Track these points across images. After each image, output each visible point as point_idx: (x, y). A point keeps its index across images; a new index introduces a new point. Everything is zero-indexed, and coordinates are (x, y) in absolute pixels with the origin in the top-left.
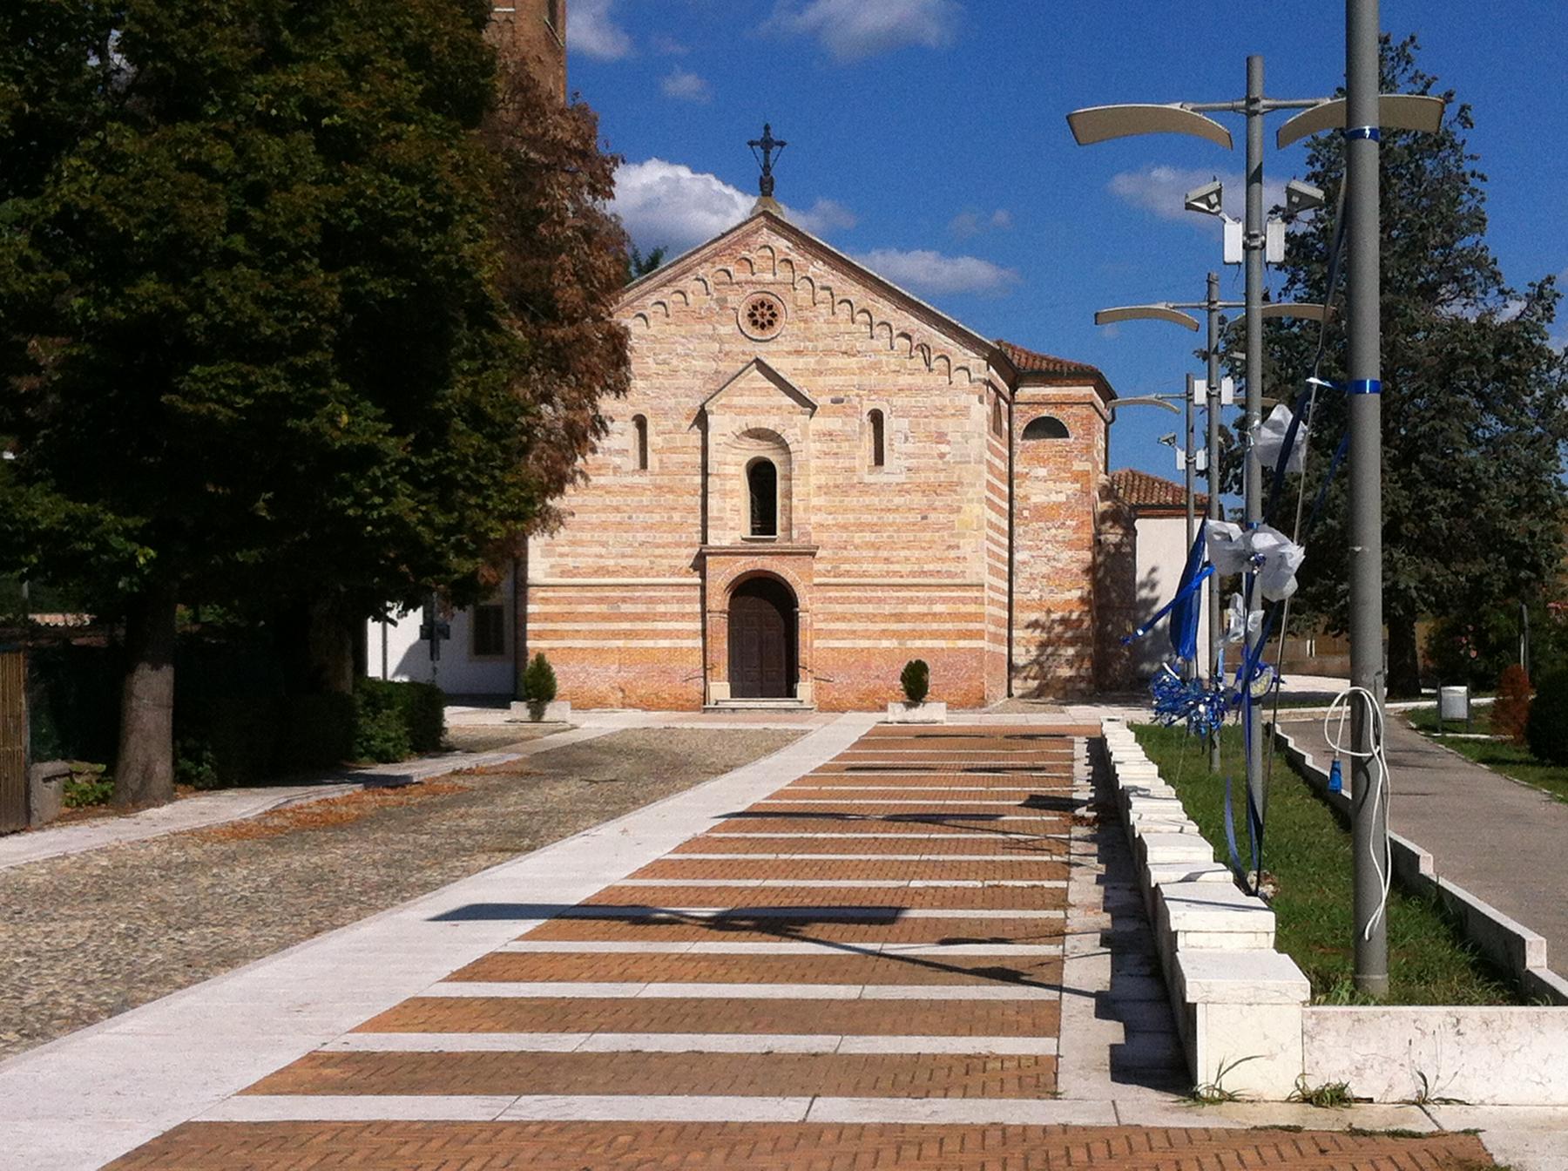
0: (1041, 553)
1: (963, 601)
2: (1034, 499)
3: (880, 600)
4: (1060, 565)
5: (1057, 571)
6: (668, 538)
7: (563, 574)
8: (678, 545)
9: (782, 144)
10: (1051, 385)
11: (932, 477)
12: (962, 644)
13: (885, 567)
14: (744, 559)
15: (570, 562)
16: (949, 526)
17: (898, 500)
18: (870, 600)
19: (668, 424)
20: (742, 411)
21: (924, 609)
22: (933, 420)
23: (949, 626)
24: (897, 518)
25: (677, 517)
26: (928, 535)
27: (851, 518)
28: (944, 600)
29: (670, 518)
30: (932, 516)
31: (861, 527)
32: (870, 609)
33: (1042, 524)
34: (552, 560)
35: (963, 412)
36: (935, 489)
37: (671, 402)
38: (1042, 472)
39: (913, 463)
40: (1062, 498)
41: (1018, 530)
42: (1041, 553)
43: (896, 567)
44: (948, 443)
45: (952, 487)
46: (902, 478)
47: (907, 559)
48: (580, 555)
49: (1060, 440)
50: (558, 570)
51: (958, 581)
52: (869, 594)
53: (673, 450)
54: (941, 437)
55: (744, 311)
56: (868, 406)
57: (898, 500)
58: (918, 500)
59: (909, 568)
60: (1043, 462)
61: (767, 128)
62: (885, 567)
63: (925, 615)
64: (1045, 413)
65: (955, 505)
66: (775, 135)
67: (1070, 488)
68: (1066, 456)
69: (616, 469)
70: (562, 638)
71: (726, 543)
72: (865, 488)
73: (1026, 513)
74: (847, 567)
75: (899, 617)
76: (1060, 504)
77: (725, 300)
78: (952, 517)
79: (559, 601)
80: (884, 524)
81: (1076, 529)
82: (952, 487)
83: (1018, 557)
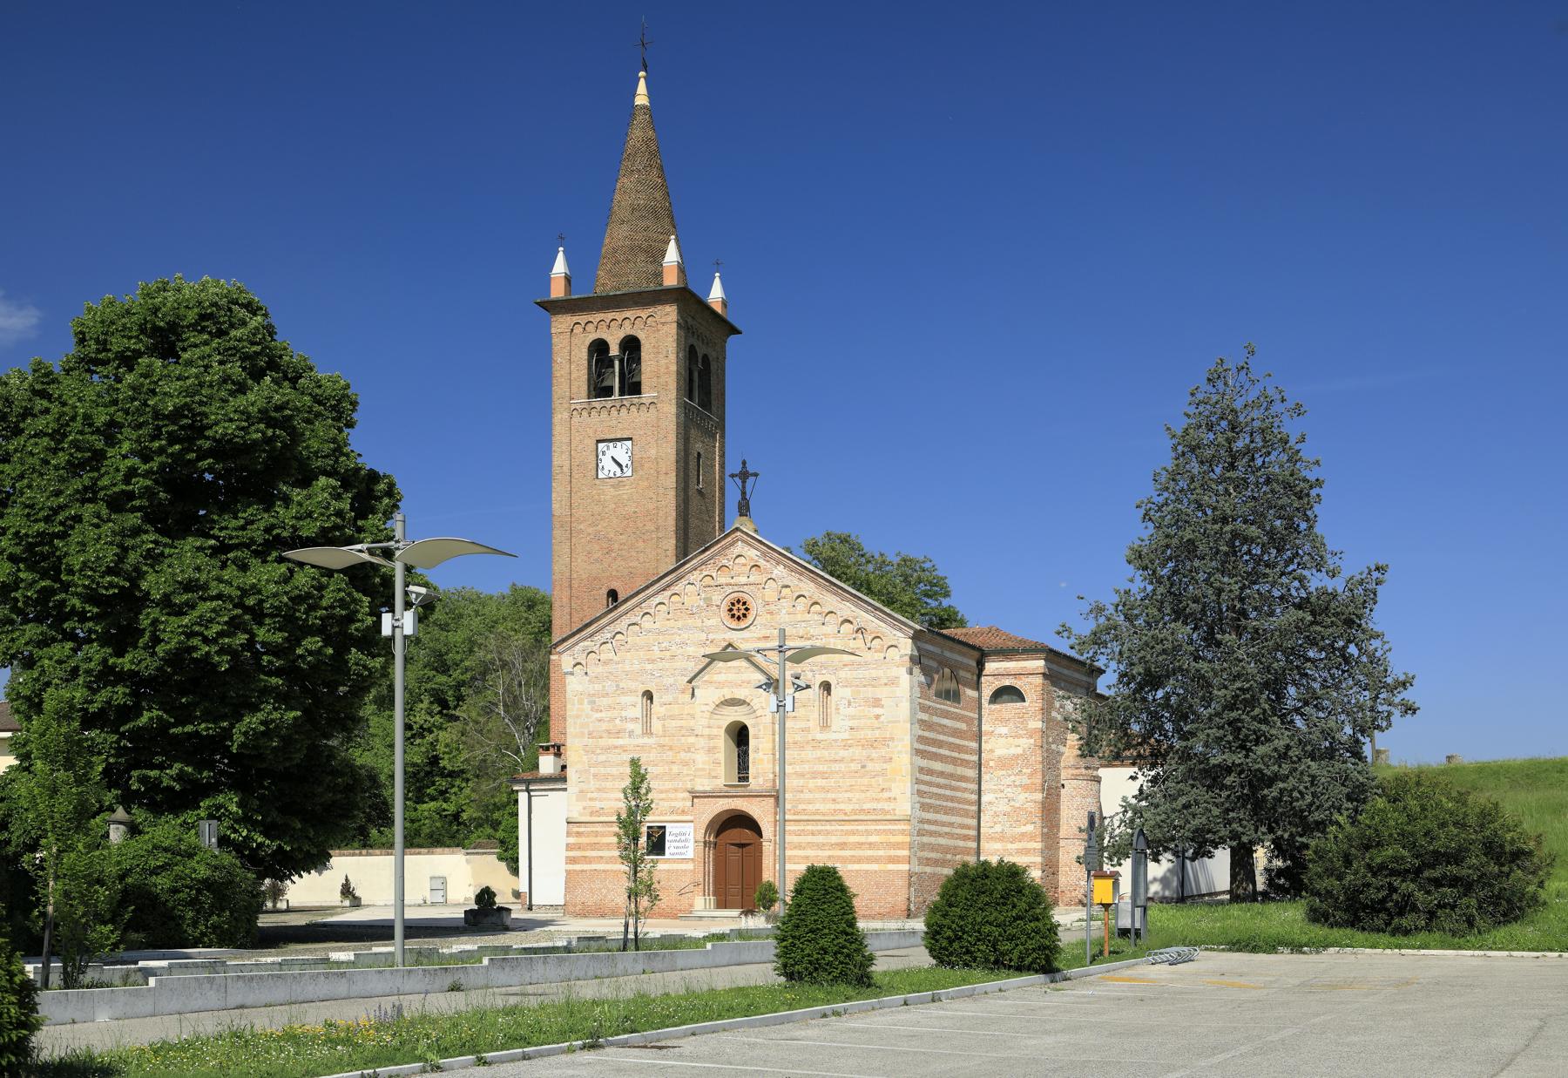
1: (892, 832)
2: (998, 752)
3: (828, 833)
5: (1015, 809)
6: (669, 785)
7: (592, 814)
8: (676, 790)
9: (756, 475)
11: (870, 734)
12: (891, 867)
15: (598, 805)
16: (883, 773)
17: (842, 753)
19: (668, 698)
20: (720, 685)
21: (862, 839)
23: (881, 853)
25: (675, 769)
26: (865, 781)
27: (806, 767)
28: (878, 832)
30: (870, 766)
31: (815, 775)
32: (820, 839)
35: (893, 682)
36: (872, 744)
37: (671, 681)
38: (1004, 730)
40: (1019, 751)
41: (985, 777)
43: (842, 806)
45: (885, 741)
46: (846, 736)
49: (1019, 704)
53: (672, 717)
54: (877, 703)
55: (725, 606)
56: (819, 679)
57: (842, 753)
58: (857, 752)
61: (744, 463)
64: (1007, 682)
66: (751, 469)
71: (708, 788)
72: (816, 744)
79: (588, 834)
81: (1031, 776)
82: (885, 741)
83: (984, 799)
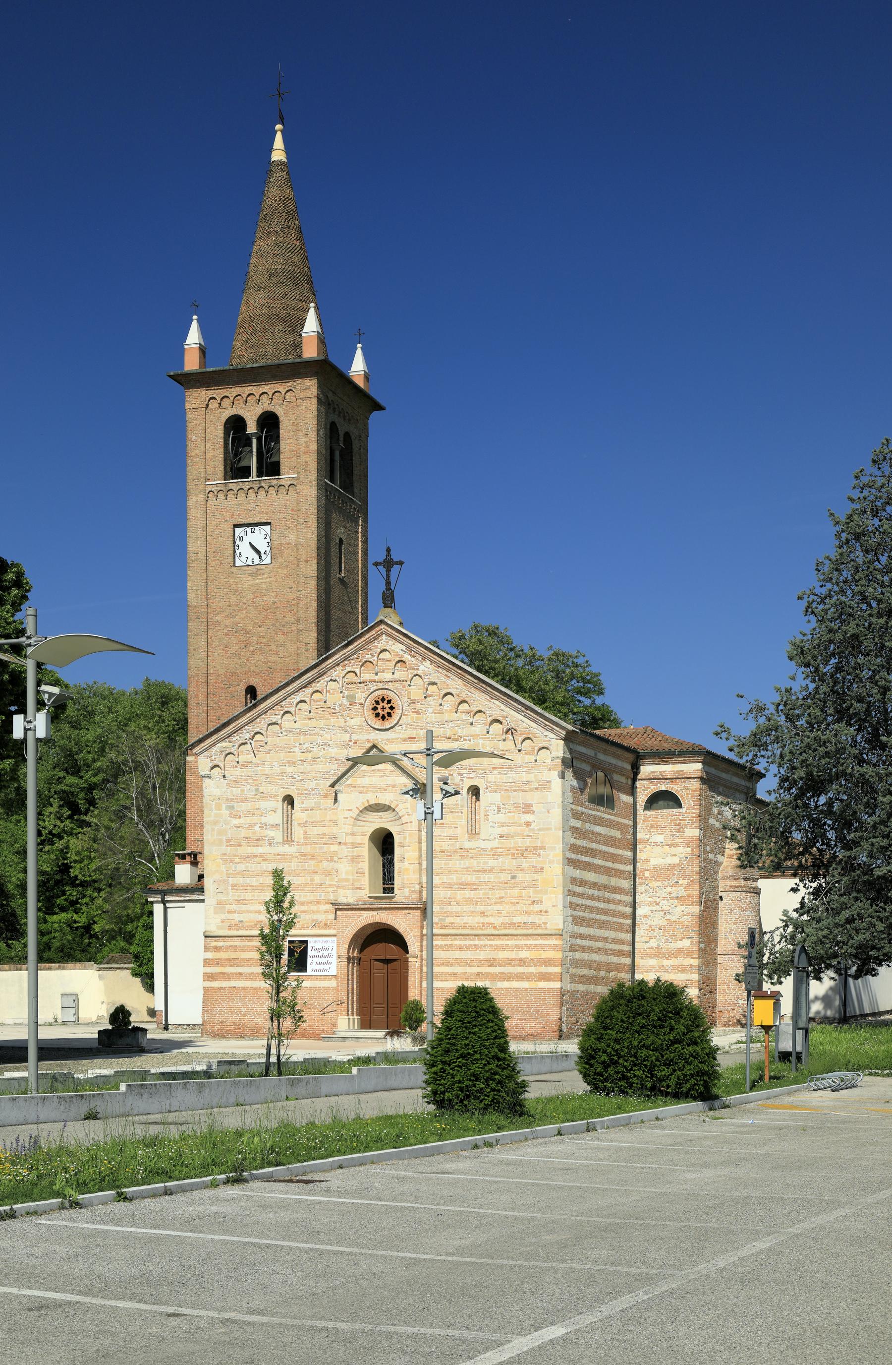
0: (657, 908)
3: (477, 948)
4: (673, 918)
5: (671, 923)
7: (230, 927)
8: (318, 902)
9: (401, 563)
10: (667, 763)
11: (520, 843)
12: (542, 984)
13: (482, 920)
14: (366, 914)
15: (236, 917)
16: (534, 884)
17: (492, 863)
18: (468, 948)
19: (309, 803)
20: (364, 790)
22: (520, 794)
23: (532, 970)
24: (492, 877)
25: (317, 879)
26: (516, 893)
27: (454, 878)
28: (529, 948)
29: (312, 880)
30: (520, 876)
31: (463, 886)
32: (468, 955)
33: (659, 883)
34: (223, 916)
36: (522, 853)
37: (312, 784)
38: (659, 838)
39: (504, 831)
40: (676, 860)
41: (640, 889)
42: (657, 908)
43: (491, 920)
44: (533, 813)
45: (536, 850)
46: (495, 844)
47: (499, 912)
48: (244, 911)
50: (227, 924)
51: (540, 931)
52: (468, 943)
53: (314, 824)
54: (527, 809)
55: (369, 705)
57: (492, 863)
58: (507, 862)
59: (501, 920)
60: (660, 829)
62: (482, 920)
63: (512, 960)
64: (663, 787)
65: (539, 866)
66: (395, 557)
67: (683, 852)
68: (679, 824)
69: (271, 841)
70: (229, 979)
71: (352, 900)
72: (465, 852)
73: (647, 874)
74: (448, 920)
75: (492, 962)
76: (673, 867)
77: (353, 697)
78: (536, 876)
80: (481, 883)
81: (687, 887)
83: (639, 912)
